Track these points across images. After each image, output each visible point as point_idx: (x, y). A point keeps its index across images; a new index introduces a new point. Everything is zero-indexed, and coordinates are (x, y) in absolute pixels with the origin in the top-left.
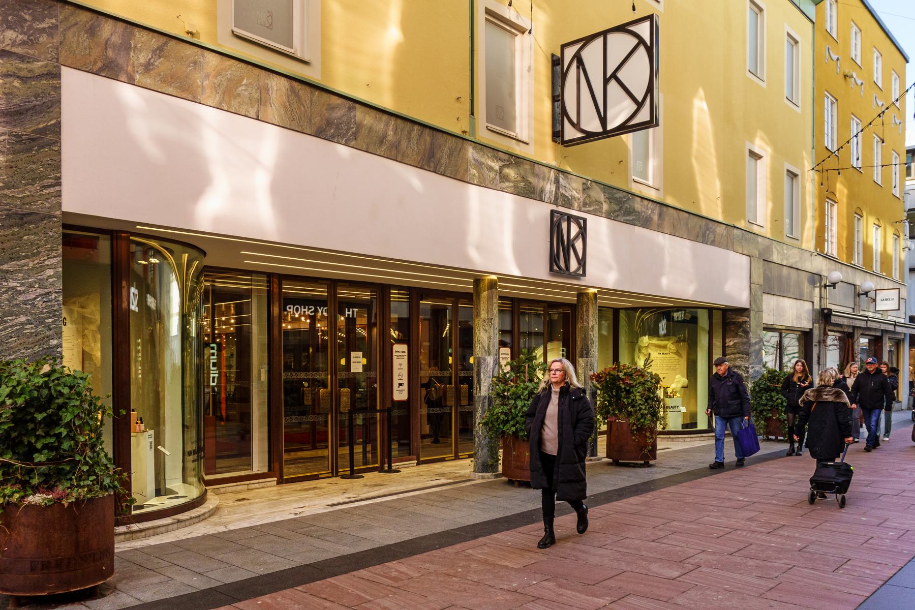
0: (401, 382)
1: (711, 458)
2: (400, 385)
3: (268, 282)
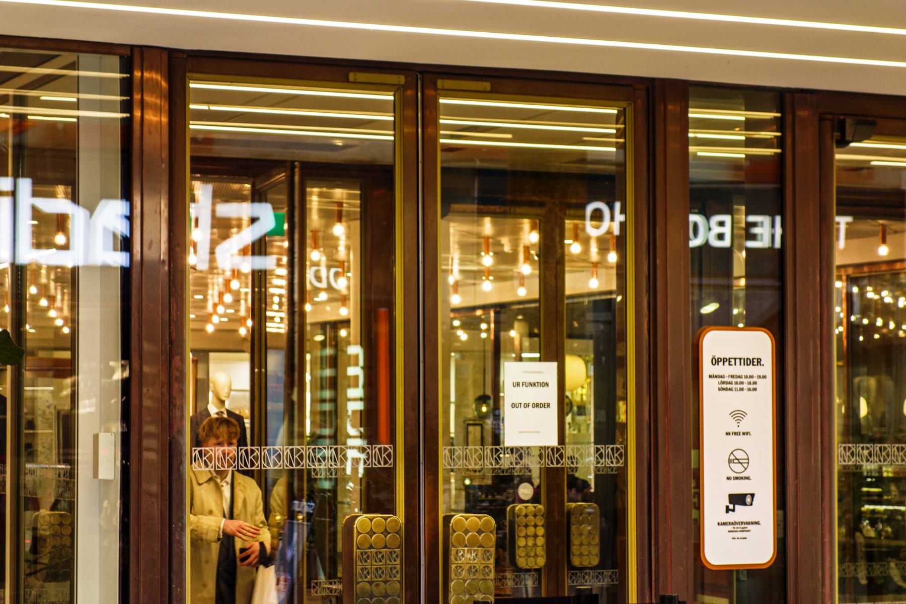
0: (739, 488)
1: (233, 388)
2: (738, 500)
3: (127, 87)
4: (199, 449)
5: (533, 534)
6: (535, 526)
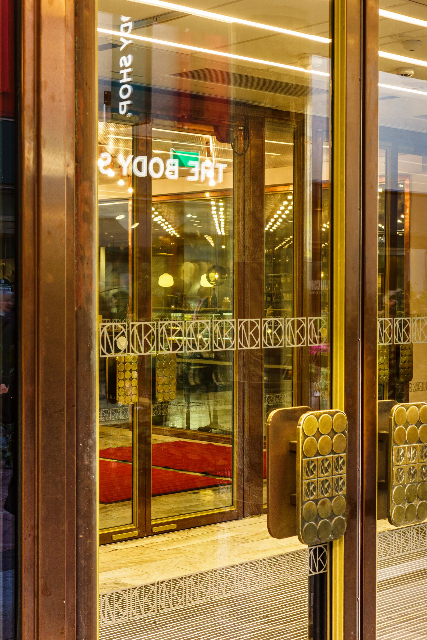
4: (315, 318)
5: (129, 377)
6: (131, 371)
